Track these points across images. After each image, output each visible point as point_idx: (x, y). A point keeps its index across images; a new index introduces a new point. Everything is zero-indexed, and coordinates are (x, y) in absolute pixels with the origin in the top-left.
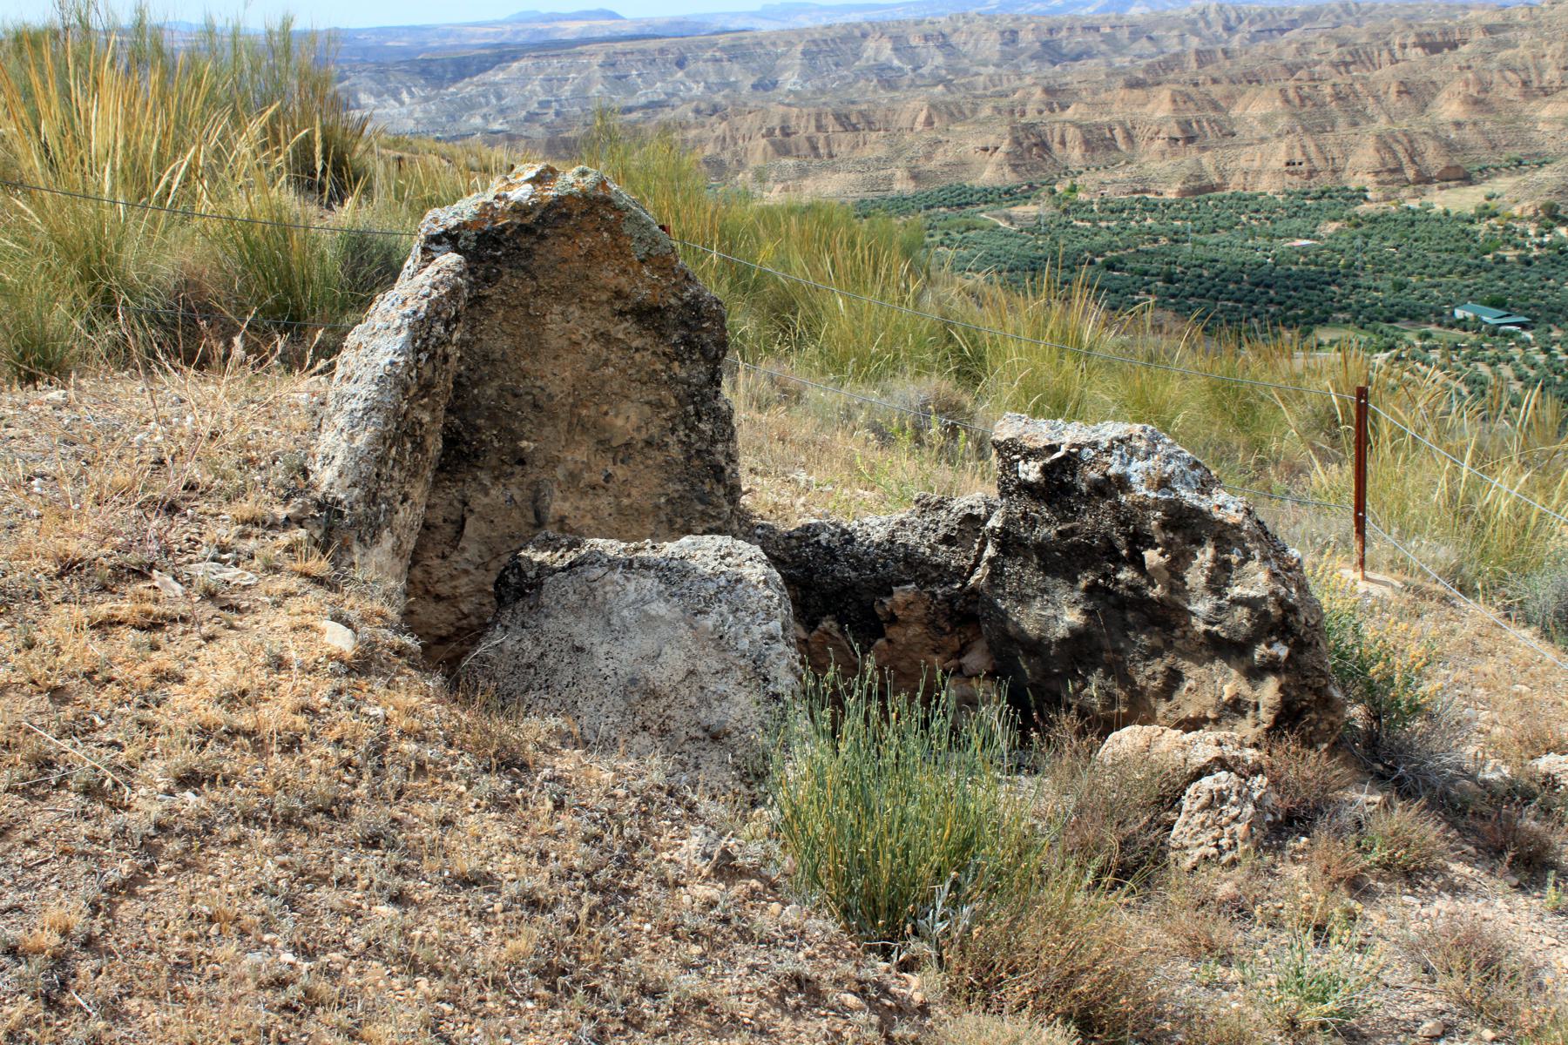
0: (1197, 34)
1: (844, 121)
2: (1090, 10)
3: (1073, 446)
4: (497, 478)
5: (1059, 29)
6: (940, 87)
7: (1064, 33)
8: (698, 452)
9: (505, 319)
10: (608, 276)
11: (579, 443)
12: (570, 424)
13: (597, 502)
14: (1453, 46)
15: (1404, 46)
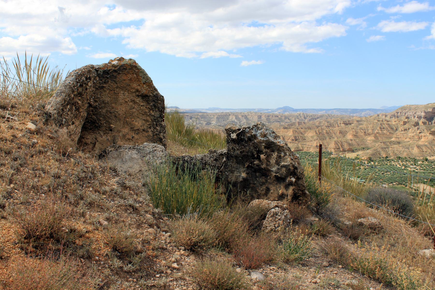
0: (298, 119)
2: (277, 113)
3: (244, 128)
4: (105, 134)
5: (270, 116)
7: (271, 117)
8: (156, 134)
9: (109, 93)
10: (135, 85)
11: (126, 128)
12: (124, 122)
14: (350, 124)
15: (340, 124)
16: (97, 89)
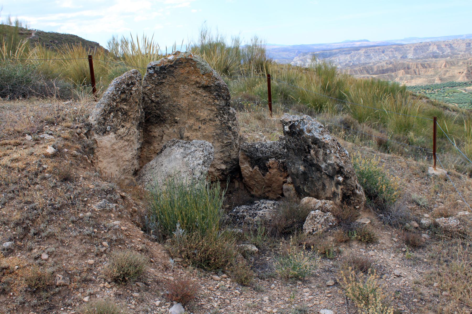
1: (423, 66)
4: (171, 126)
6: (449, 57)
8: (224, 123)
10: (193, 77)
13: (197, 134)
16: (157, 85)
